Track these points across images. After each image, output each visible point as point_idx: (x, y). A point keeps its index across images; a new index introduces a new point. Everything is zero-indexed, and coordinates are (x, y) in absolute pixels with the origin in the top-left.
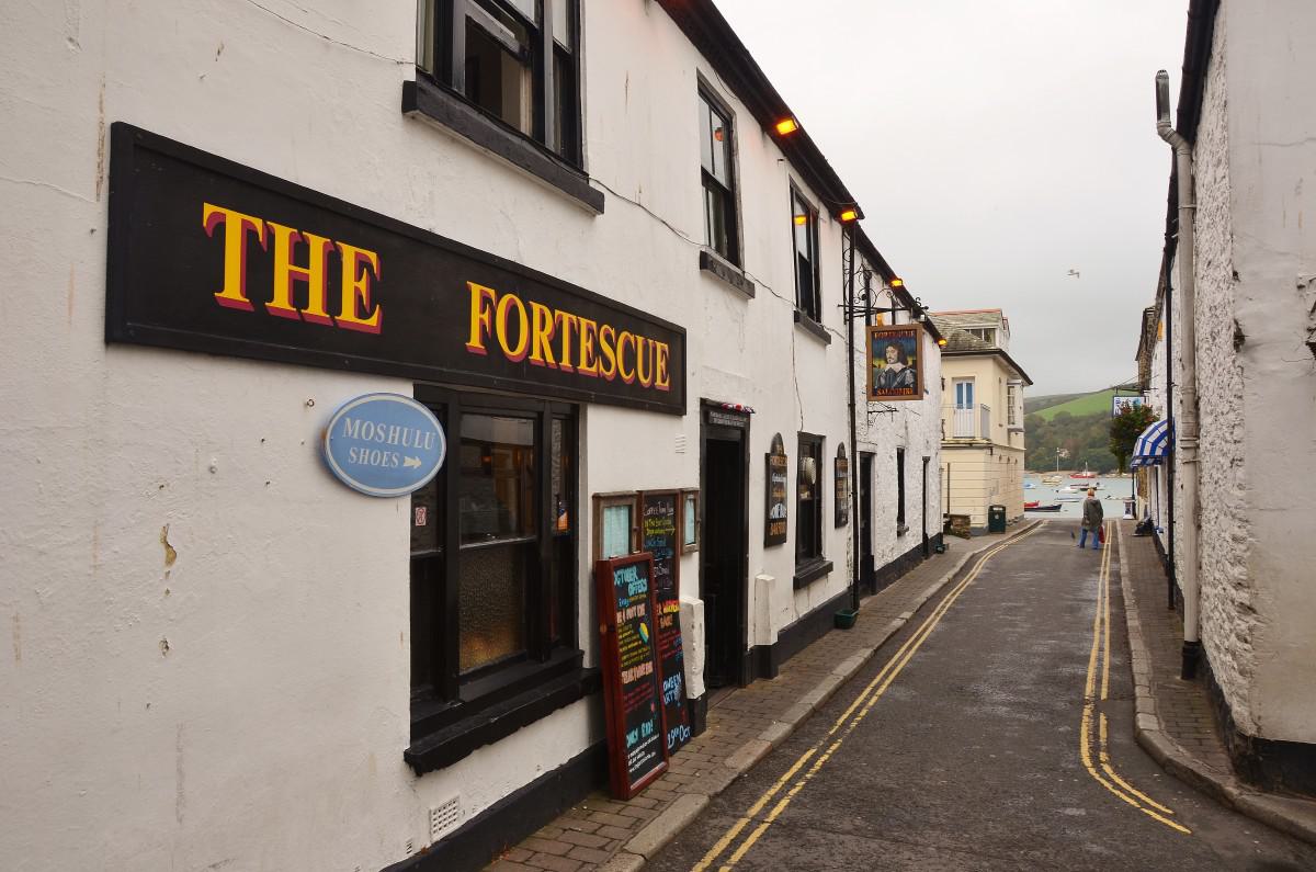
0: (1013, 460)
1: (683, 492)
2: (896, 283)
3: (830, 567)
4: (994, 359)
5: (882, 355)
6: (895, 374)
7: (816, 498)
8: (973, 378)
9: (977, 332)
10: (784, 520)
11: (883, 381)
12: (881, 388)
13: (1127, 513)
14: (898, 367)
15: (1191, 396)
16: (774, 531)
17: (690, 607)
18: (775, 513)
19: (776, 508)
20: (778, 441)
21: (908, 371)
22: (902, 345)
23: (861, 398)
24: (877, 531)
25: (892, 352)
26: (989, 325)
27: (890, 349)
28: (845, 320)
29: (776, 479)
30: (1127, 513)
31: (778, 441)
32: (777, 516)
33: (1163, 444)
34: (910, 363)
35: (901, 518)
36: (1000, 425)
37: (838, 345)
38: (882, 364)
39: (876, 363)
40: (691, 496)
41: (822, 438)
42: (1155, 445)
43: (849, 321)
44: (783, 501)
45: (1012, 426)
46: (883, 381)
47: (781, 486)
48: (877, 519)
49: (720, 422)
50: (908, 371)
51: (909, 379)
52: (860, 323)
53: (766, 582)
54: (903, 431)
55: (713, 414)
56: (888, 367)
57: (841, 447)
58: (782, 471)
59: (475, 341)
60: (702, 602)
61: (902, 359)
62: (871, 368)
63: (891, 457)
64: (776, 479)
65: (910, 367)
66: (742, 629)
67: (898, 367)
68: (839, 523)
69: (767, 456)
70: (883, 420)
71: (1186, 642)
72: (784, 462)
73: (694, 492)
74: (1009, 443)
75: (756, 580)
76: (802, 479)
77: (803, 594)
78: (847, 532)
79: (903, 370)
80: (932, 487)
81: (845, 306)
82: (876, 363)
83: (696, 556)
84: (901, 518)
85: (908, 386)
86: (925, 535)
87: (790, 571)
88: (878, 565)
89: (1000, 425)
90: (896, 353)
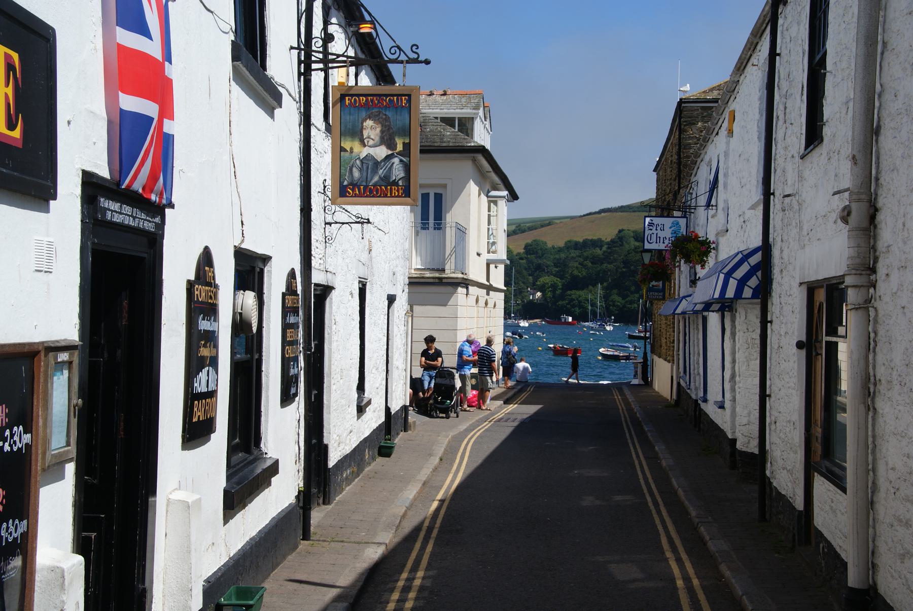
0: (491, 304)
1: (53, 348)
2: (365, 29)
3: (274, 469)
4: (474, 161)
5: (356, 133)
6: (376, 164)
7: (256, 356)
8: (444, 186)
9: (449, 121)
10: (211, 394)
11: (356, 174)
12: (354, 185)
13: (635, 376)
14: (381, 152)
15: (864, 206)
16: (199, 415)
17: (59, 574)
18: (200, 385)
19: (203, 375)
20: (206, 259)
21: (396, 160)
22: (387, 119)
23: (317, 201)
24: (333, 406)
25: (371, 129)
26: (467, 112)
27: (369, 123)
28: (300, 74)
29: (204, 325)
30: (635, 376)
31: (206, 259)
32: (204, 390)
33: (753, 282)
34: (400, 147)
35: (361, 387)
36: (479, 255)
37: (289, 110)
38: (357, 147)
39: (347, 145)
40: (64, 357)
41: (266, 259)
42: (742, 283)
43: (305, 74)
44: (214, 362)
45: (492, 256)
46: (356, 174)
47: (211, 338)
48: (333, 387)
49: (117, 219)
50: (396, 160)
51: (398, 172)
52: (317, 78)
53: (187, 506)
54: (364, 257)
55: (105, 203)
56: (365, 152)
57: (292, 275)
58: (211, 310)
59: (6, 436)
60: (80, 559)
61: (387, 140)
62: (339, 151)
63: (351, 294)
64: (204, 325)
65: (400, 153)
66: (144, 591)
67: (381, 152)
68: (287, 398)
69: (190, 286)
70: (348, 236)
71: (852, 589)
72: (216, 295)
73: (68, 348)
74: (488, 280)
75: (168, 500)
76: (240, 326)
77: (239, 518)
78: (298, 407)
79: (388, 158)
80: (691, 363)
81: (298, 48)
82: (347, 145)
83: (70, 469)
84: (361, 387)
85: (395, 183)
86: (388, 409)
87: (220, 481)
88: (333, 458)
89: (479, 255)
90: (378, 130)
